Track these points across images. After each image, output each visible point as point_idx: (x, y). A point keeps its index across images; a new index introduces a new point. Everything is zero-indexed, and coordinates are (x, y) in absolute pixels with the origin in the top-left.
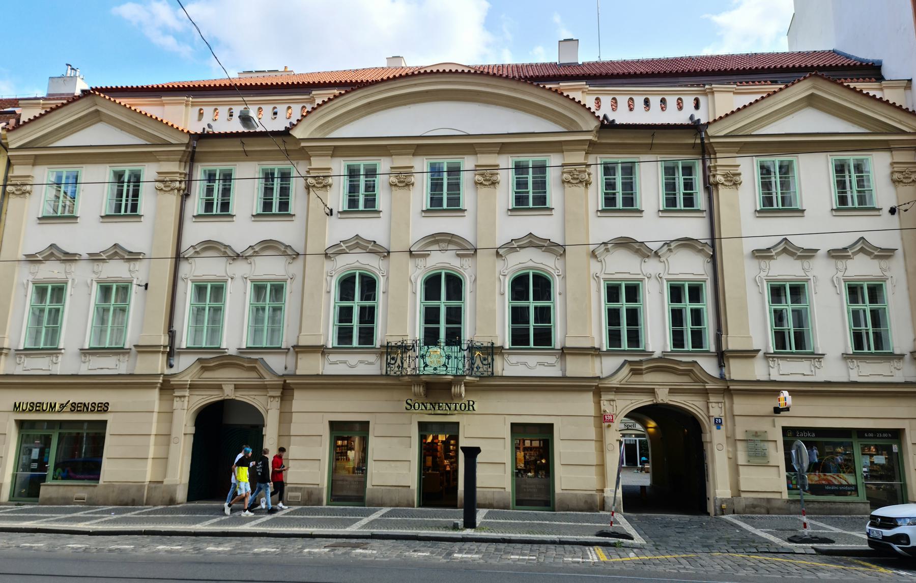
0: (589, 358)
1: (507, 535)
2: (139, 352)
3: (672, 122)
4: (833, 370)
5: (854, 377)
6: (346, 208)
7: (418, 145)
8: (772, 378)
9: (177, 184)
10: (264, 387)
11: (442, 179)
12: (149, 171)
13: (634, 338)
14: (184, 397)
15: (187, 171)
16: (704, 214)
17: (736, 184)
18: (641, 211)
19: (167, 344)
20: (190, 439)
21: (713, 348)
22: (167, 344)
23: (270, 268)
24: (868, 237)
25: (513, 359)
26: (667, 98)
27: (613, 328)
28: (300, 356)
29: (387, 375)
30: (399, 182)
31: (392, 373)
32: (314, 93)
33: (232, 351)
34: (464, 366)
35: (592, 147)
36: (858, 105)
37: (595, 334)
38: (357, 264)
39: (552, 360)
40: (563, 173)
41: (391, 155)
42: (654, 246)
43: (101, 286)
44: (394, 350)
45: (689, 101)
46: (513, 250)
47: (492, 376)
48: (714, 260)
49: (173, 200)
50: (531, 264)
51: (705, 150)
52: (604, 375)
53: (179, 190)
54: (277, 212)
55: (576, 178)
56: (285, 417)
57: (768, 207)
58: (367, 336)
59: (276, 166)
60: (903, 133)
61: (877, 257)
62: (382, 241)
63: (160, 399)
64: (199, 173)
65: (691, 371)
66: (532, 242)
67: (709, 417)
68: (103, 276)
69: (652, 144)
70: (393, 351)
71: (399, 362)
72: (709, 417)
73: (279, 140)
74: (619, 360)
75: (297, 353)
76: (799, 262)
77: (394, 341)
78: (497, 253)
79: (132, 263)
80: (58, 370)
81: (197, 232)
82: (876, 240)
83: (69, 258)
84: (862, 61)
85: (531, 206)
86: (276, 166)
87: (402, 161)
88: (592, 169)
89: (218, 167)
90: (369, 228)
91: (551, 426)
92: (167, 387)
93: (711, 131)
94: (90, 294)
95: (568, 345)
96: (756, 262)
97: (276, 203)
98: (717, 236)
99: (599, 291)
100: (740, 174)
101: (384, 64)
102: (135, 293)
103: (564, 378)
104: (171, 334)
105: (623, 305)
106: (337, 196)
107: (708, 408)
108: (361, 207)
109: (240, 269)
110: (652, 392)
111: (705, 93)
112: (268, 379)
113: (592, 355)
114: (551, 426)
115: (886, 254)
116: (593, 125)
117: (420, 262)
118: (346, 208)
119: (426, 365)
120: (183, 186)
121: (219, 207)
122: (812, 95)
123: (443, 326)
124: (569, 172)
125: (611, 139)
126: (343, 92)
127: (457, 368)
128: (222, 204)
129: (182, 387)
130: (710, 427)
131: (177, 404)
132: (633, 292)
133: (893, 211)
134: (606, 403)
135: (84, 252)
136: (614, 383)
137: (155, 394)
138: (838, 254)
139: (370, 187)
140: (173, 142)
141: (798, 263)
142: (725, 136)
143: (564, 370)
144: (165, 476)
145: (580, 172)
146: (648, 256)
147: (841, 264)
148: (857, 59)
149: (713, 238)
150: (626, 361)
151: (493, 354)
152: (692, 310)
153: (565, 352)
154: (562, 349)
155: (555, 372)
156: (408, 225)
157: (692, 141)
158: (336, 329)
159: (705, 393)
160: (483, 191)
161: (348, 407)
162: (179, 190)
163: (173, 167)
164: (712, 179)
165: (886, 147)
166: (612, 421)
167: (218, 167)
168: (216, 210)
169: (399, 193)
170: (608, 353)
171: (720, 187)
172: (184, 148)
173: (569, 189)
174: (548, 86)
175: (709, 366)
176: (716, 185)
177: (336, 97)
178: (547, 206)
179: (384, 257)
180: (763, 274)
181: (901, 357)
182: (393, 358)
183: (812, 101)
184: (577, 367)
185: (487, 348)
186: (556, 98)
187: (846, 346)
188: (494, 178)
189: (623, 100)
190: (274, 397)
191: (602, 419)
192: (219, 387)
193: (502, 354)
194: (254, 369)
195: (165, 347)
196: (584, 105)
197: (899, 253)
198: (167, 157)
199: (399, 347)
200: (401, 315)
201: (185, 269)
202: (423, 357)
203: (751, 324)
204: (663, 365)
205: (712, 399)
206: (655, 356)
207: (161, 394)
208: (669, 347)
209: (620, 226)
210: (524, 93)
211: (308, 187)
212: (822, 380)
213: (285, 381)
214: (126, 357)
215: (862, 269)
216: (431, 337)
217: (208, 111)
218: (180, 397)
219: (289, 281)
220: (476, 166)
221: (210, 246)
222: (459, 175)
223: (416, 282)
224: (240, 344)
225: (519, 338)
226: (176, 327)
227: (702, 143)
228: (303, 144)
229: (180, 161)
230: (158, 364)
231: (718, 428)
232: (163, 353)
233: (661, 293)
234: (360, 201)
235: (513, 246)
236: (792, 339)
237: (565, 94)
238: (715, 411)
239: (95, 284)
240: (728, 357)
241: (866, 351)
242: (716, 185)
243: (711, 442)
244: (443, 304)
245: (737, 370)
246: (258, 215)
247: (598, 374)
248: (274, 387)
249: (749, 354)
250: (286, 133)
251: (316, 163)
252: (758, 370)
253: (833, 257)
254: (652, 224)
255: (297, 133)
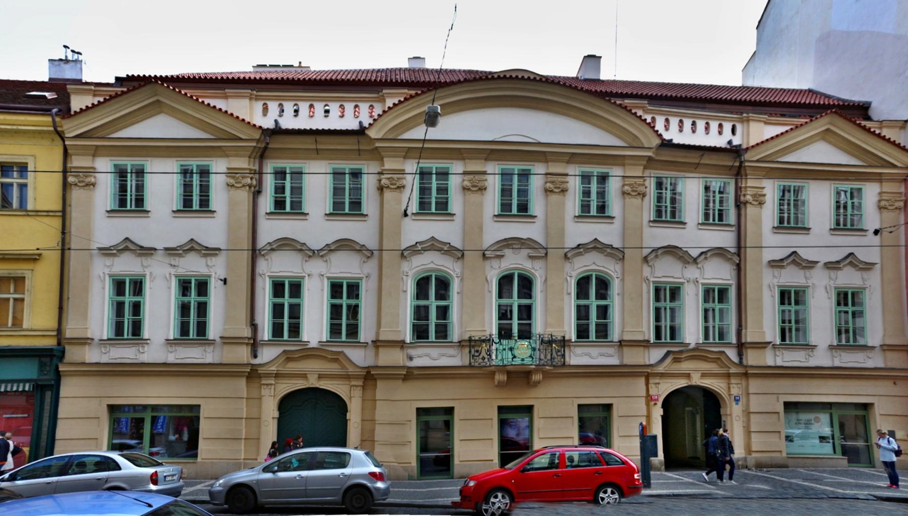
0: (642, 349)
1: (676, 491)
2: (225, 343)
3: (687, 143)
4: (821, 359)
5: (837, 363)
6: (273, 210)
7: (492, 150)
8: (778, 364)
9: (249, 181)
10: (347, 377)
11: (431, 183)
12: (219, 166)
13: (295, 330)
14: (271, 384)
15: (257, 167)
16: (733, 229)
17: (761, 204)
18: (685, 224)
19: (250, 336)
20: (276, 421)
21: (734, 341)
22: (250, 336)
23: (346, 267)
24: (801, 252)
25: (579, 350)
26: (685, 120)
27: (293, 321)
28: (381, 349)
29: (471, 366)
30: (633, 191)
31: (476, 364)
32: (384, 91)
33: (314, 344)
34: (545, 357)
35: (650, 163)
36: (863, 142)
37: (645, 329)
38: (432, 266)
39: (611, 351)
40: (464, 180)
41: (227, 156)
42: (694, 253)
43: (179, 280)
44: (478, 343)
45: (727, 127)
46: (418, 252)
47: (564, 365)
48: (739, 269)
49: (244, 196)
50: (594, 267)
51: (739, 173)
52: (652, 362)
53: (250, 186)
54: (198, 208)
55: (632, 192)
56: (369, 404)
57: (784, 225)
58: (443, 332)
59: (347, 166)
60: (894, 166)
61: (861, 269)
62: (457, 243)
63: (247, 387)
64: (269, 166)
65: (337, 358)
66: (596, 246)
67: (730, 395)
68: (181, 271)
69: (698, 164)
70: (471, 344)
71: (483, 354)
72: (730, 395)
73: (353, 139)
74: (664, 351)
75: (377, 347)
76: (802, 272)
77: (477, 336)
78: (484, 255)
79: (209, 258)
80: (812, 363)
81: (272, 229)
82: (863, 255)
83: (146, 251)
84: (844, 101)
85: (347, 211)
86: (347, 166)
87: (475, 166)
88: (490, 178)
89: (289, 165)
90: (608, 233)
91: (198, 407)
92: (253, 374)
93: (747, 156)
94: (170, 288)
95: (625, 338)
96: (827, 272)
97: (346, 204)
98: (743, 245)
99: (649, 292)
100: (764, 195)
101: (405, 65)
102: (215, 288)
103: (622, 366)
104: (254, 327)
105: (128, 299)
106: (411, 197)
107: (729, 388)
108: (288, 209)
109: (316, 267)
110: (688, 376)
111: (742, 121)
112: (351, 369)
113: (644, 346)
114: (198, 407)
115: (868, 267)
116: (656, 142)
117: (495, 263)
118: (273, 210)
119: (514, 357)
120: (254, 182)
121: (288, 204)
122: (828, 130)
123: (515, 322)
124: (629, 185)
125: (667, 155)
126: (419, 92)
127: (540, 359)
128: (137, 200)
129: (268, 375)
130: (730, 403)
131: (265, 391)
132: (296, 289)
133: (876, 232)
134: (653, 386)
135: (159, 245)
136: (661, 369)
137: (243, 382)
138: (832, 266)
139: (443, 190)
140: (243, 137)
141: (859, 274)
142: (758, 161)
143: (622, 360)
144: (258, 455)
145: (640, 185)
146: (688, 263)
147: (833, 273)
148: (839, 99)
149: (739, 247)
150: (668, 353)
151: (564, 346)
152: (598, 307)
153: (622, 344)
154: (459, 342)
155: (614, 361)
156: (481, 228)
157: (731, 164)
158: (271, 323)
159: (728, 376)
160: (554, 198)
161: (435, 396)
162: (250, 186)
163: (242, 163)
164: (742, 198)
165: (878, 178)
166: (657, 400)
167: (289, 165)
168: (130, 205)
169: (474, 197)
170: (655, 345)
171: (748, 205)
172: (254, 144)
173: (629, 200)
174: (618, 102)
175: (732, 354)
176: (746, 203)
177: (412, 97)
178: (449, 211)
179: (459, 258)
180: (775, 281)
181: (873, 348)
182: (477, 351)
183: (827, 135)
184: (634, 357)
185: (560, 341)
186: (623, 114)
187: (698, 338)
188: (564, 186)
189: (674, 122)
190: (357, 386)
191: (649, 399)
192: (688, 376)
193: (569, 346)
194: (336, 360)
195: (249, 339)
196: (226, 112)
197: (878, 267)
198: (235, 152)
199: (484, 341)
200: (475, 312)
201: (262, 266)
202: (511, 349)
203: (766, 322)
204: (697, 354)
205: (733, 381)
206: (691, 347)
207: (247, 382)
208: (325, 336)
209: (129, 227)
210: (582, 101)
211: (381, 189)
212: (94, 361)
213: (368, 373)
214: (211, 348)
215: (848, 278)
216: (505, 333)
217: (273, 106)
218: (267, 385)
219: (364, 280)
220: (228, 169)
221: (285, 244)
222: (143, 177)
223: (492, 282)
224: (102, 335)
225: (582, 333)
226: (258, 320)
227: (740, 166)
228: (377, 145)
229: (249, 157)
230: (242, 354)
231: (737, 404)
232: (247, 344)
233: (697, 295)
234: (432, 203)
235: (581, 249)
236: (792, 331)
237: (633, 111)
238: (735, 391)
239: (173, 279)
240: (746, 348)
241: (663, 341)
242: (746, 203)
243: (730, 415)
244: (287, 300)
245: (753, 358)
246: (178, 211)
247: (647, 363)
248: (356, 377)
249: (762, 346)
250: (361, 132)
251: (389, 164)
252: (769, 359)
253: (828, 268)
254: (694, 236)
255: (372, 133)
